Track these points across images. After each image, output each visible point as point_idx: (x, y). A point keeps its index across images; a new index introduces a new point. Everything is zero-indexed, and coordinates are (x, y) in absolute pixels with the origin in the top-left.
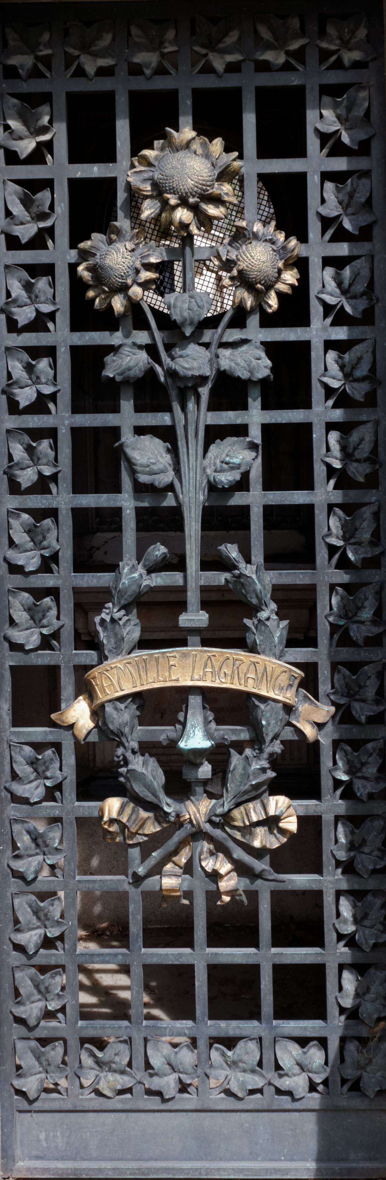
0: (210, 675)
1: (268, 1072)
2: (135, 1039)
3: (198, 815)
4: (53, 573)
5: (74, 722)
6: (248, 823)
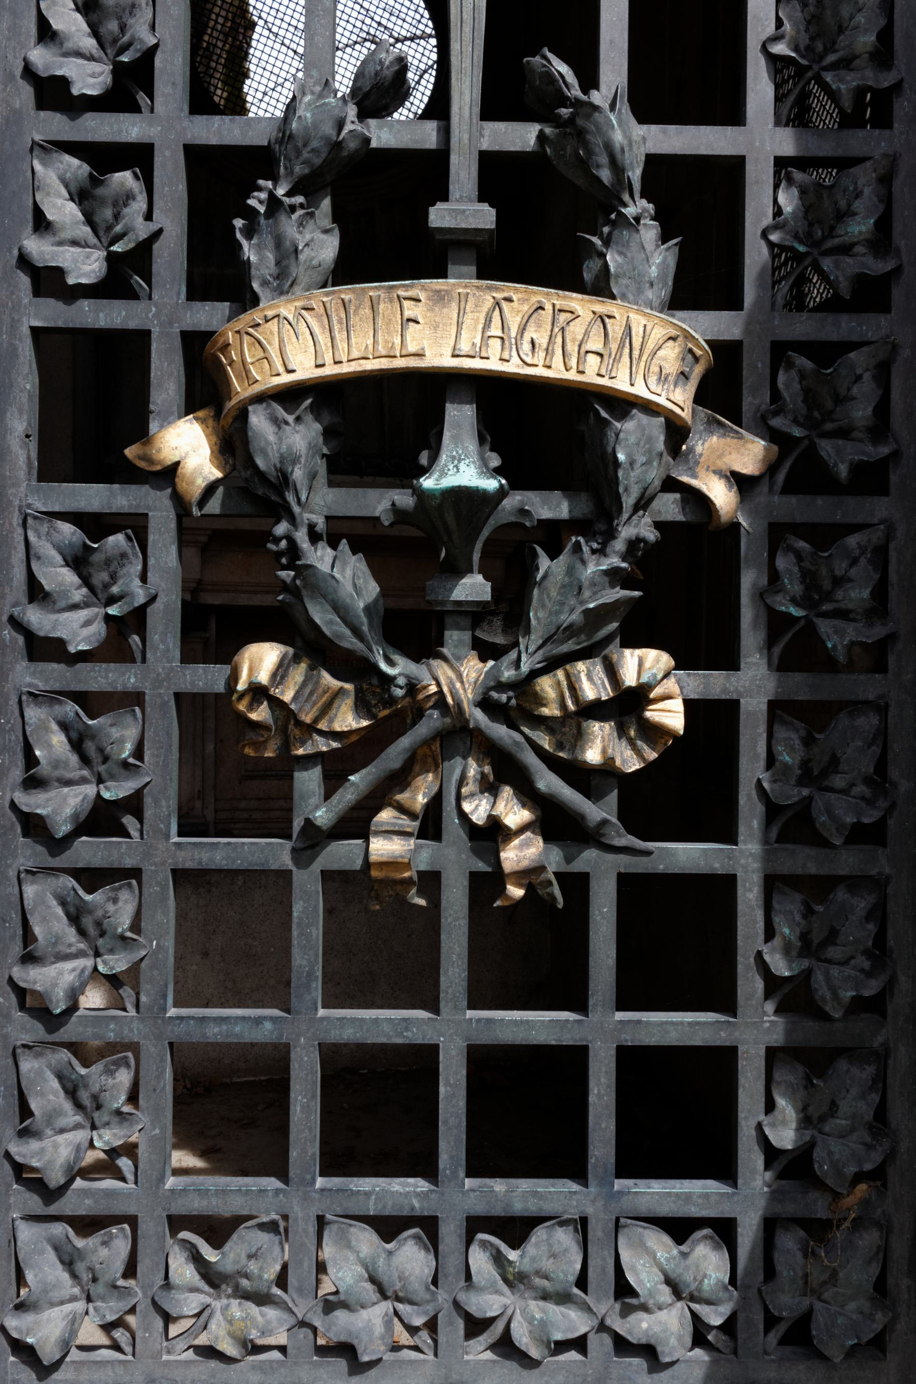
0: (496, 344)
1: (599, 1300)
2: (296, 1219)
3: (458, 685)
4: (140, 111)
5: (177, 459)
6: (571, 706)
